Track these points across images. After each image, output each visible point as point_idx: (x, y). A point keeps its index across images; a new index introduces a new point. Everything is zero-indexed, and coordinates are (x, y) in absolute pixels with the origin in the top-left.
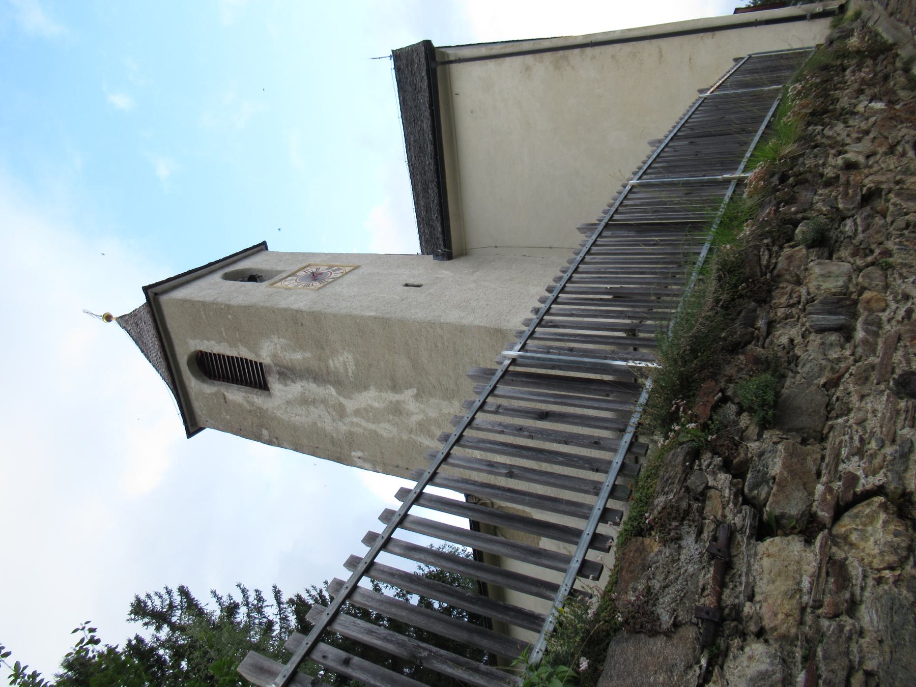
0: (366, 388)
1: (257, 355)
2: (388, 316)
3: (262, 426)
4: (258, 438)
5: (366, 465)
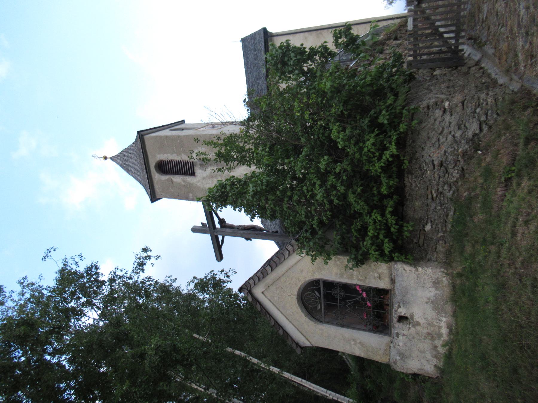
3: (189, 192)
4: (187, 198)
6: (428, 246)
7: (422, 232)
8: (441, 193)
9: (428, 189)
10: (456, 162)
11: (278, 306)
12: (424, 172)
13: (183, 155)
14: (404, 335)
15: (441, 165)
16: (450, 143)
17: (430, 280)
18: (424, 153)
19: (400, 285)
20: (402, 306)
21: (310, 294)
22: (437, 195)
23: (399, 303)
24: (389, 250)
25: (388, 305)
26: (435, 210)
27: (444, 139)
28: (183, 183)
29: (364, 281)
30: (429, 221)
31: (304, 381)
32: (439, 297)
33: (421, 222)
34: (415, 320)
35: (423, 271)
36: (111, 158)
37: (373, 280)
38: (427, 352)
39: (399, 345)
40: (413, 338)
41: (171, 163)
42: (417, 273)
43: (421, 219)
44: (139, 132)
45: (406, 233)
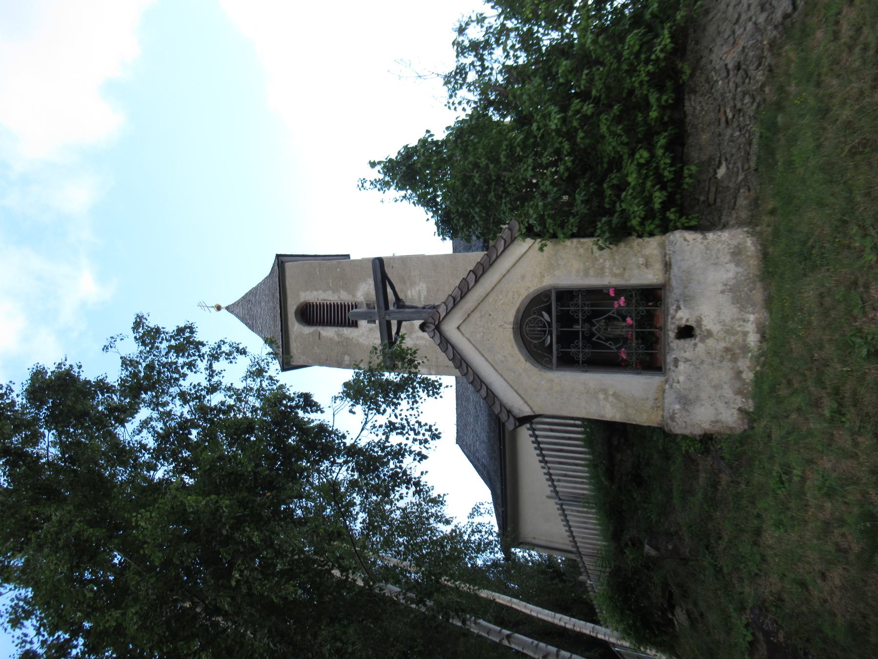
1: (354, 296)
6: (722, 201)
7: (713, 180)
8: (740, 110)
9: (719, 111)
10: (761, 59)
11: (481, 349)
12: (712, 84)
13: (342, 292)
14: (687, 360)
15: (738, 67)
16: (750, 33)
17: (726, 251)
18: (714, 57)
19: (679, 268)
20: (682, 307)
21: (535, 319)
22: (734, 116)
23: (678, 301)
24: (660, 201)
25: (661, 328)
26: (732, 140)
27: (742, 30)
28: (336, 338)
29: (621, 275)
30: (723, 159)
31: (514, 600)
32: (743, 278)
33: (711, 164)
34: (704, 328)
35: (716, 236)
36: (227, 308)
37: (636, 272)
38: (725, 386)
39: (678, 382)
40: (702, 362)
41: (320, 307)
42: (705, 242)
43: (711, 159)
44: (278, 256)
45: (688, 180)
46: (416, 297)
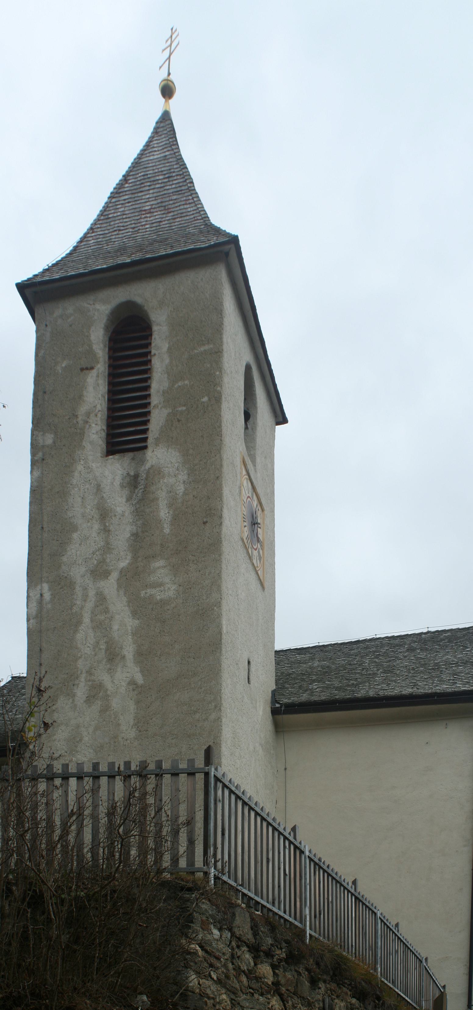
0: (135, 614)
1: (157, 442)
2: (224, 650)
5: (34, 604)
13: (166, 412)
46: (153, 578)
